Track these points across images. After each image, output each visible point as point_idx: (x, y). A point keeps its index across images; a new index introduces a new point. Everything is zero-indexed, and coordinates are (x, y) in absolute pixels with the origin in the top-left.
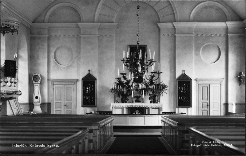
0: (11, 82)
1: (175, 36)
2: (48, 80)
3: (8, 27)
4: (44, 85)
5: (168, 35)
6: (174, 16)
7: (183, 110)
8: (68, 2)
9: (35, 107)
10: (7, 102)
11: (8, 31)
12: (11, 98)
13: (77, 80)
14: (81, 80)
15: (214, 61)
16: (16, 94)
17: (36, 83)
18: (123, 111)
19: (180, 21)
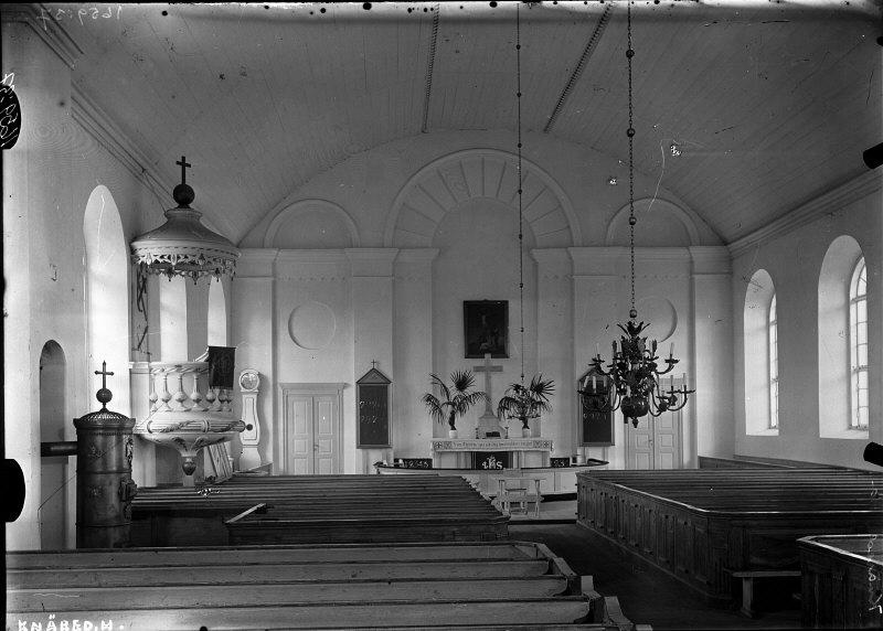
0: (222, 401)
1: (572, 281)
2: (275, 385)
3: (161, 261)
4: (28, 403)
5: (557, 277)
6: (571, 234)
7: (595, 453)
8: (666, 201)
9: (743, 450)
10: (205, 449)
11: (206, 273)
12: (222, 440)
13: (346, 386)
14: (354, 384)
15: (668, 333)
16: (234, 430)
17: (247, 393)
18: (458, 462)
19: (735, 241)
